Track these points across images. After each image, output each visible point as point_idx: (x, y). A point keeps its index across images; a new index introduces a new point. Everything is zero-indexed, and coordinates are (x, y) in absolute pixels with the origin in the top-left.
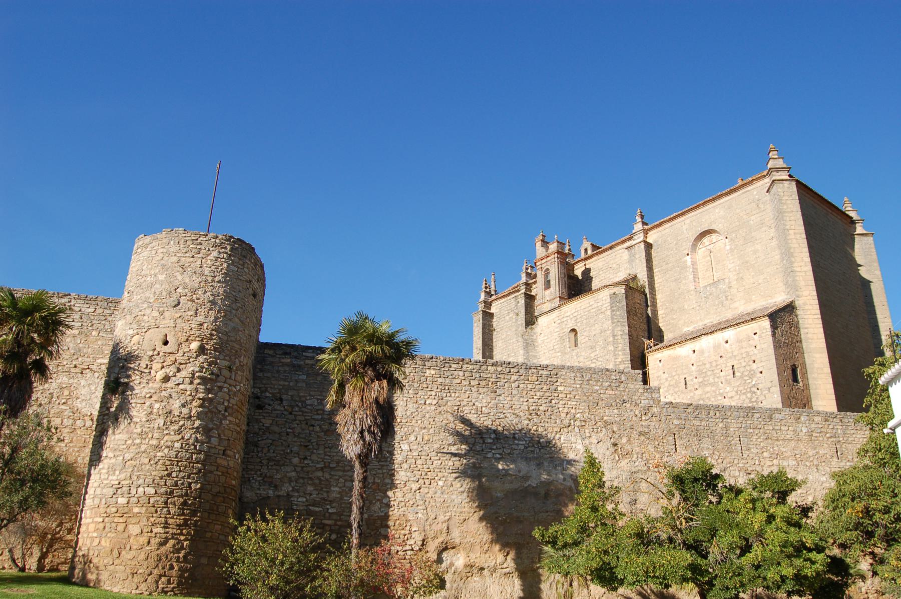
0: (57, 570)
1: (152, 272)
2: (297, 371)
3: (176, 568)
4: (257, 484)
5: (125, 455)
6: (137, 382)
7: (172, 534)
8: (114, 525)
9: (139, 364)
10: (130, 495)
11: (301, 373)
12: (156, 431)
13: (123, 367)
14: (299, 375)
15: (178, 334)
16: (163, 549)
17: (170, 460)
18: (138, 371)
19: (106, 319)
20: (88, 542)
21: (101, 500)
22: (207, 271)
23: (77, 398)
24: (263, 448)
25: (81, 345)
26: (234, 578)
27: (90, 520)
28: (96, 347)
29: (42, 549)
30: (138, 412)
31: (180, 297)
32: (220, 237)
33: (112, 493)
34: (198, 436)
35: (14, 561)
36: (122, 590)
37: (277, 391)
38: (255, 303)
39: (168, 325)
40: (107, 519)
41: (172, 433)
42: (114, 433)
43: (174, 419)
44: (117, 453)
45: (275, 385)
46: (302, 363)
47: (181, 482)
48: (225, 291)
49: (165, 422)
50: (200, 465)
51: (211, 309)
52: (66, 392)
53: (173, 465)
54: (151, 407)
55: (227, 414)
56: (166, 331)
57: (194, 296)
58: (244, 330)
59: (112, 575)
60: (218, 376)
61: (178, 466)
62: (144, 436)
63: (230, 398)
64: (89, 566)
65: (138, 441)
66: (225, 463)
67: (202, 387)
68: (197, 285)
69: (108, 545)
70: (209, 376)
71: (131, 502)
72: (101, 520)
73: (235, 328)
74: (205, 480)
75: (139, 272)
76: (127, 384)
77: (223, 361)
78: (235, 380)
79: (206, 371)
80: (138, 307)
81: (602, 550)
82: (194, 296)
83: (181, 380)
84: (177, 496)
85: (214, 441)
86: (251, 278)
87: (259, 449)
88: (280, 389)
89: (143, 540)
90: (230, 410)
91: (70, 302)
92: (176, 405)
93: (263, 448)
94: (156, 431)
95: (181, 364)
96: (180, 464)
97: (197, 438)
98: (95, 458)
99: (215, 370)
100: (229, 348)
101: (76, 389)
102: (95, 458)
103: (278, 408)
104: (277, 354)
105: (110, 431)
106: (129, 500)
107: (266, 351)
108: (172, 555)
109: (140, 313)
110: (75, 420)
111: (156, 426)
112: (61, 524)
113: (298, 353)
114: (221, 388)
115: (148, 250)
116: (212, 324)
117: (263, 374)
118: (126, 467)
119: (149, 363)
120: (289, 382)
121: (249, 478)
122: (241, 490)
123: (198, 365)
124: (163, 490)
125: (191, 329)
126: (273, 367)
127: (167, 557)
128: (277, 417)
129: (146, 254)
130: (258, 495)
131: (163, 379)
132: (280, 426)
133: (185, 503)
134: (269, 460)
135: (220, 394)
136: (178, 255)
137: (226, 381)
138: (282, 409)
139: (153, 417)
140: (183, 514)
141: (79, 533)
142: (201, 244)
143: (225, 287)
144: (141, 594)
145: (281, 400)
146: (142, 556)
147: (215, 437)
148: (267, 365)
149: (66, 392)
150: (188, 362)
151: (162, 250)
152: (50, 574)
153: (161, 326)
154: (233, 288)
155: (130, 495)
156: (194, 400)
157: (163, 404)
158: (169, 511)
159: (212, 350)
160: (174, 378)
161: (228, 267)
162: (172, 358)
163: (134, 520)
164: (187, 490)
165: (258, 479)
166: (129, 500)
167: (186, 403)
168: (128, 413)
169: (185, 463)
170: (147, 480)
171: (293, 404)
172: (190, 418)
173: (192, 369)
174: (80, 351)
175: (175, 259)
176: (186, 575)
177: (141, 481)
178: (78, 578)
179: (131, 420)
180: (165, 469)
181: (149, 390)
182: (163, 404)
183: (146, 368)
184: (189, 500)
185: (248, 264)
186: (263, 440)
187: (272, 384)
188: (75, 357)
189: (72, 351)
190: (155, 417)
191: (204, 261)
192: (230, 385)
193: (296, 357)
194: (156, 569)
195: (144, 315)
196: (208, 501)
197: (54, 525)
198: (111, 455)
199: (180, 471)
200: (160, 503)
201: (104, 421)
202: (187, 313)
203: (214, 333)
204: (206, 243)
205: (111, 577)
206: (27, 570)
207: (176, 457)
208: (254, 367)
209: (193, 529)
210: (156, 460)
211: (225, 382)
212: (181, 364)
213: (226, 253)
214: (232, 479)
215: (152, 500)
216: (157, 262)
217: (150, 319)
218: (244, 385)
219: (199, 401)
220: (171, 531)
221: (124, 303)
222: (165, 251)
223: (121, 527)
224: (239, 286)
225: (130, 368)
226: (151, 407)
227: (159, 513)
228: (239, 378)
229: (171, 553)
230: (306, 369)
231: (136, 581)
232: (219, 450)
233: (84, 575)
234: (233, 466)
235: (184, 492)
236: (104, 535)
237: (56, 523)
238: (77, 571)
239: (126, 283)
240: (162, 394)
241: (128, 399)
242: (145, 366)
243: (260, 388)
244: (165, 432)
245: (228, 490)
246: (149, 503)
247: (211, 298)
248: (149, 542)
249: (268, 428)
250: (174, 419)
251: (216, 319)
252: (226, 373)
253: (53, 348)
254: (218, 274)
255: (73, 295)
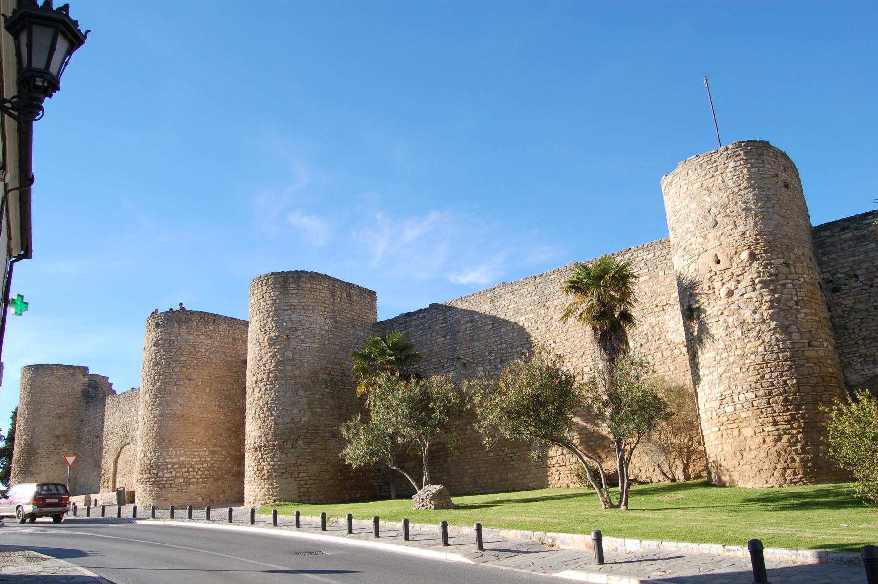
0: (701, 477)
1: (684, 205)
2: (863, 242)
3: (798, 460)
4: (859, 365)
5: (719, 370)
6: (706, 304)
7: (783, 430)
8: (729, 431)
9: (703, 288)
10: (734, 403)
11: (868, 243)
12: (737, 342)
13: (691, 295)
14: (867, 245)
15: (726, 250)
16: (779, 445)
17: (759, 364)
18: (704, 294)
19: (666, 259)
20: (714, 449)
21: (712, 412)
22: (730, 183)
23: (668, 332)
24: (853, 329)
25: (654, 287)
26: (843, 462)
27: (709, 431)
28: (666, 284)
29: (683, 461)
30: (716, 330)
31: (716, 216)
32: (730, 148)
33: (718, 405)
34: (778, 336)
35: (664, 474)
36: (754, 486)
37: (849, 268)
38: (791, 193)
39: (714, 246)
40: (722, 428)
41: (753, 340)
42: (703, 353)
43: (750, 327)
44: (711, 370)
45: (844, 263)
46: (865, 232)
47: (776, 381)
48: (754, 195)
49: (742, 332)
50: (789, 362)
51: (747, 216)
52: (657, 330)
53: (763, 368)
54: (725, 322)
55: (799, 307)
56: (714, 251)
57: (728, 211)
58: (788, 223)
59: (742, 475)
60: (777, 275)
61: (768, 368)
62: (729, 349)
63: (797, 292)
64: (720, 469)
65: (725, 355)
66: (814, 354)
67: (765, 290)
68: (726, 200)
69: (730, 449)
70: (769, 278)
71: (737, 409)
72: (717, 429)
73: (778, 225)
74: (799, 375)
75: (673, 209)
76: (699, 308)
77: (777, 260)
78: (796, 273)
79: (764, 275)
80: (684, 239)
81: (258, 446)
82: (728, 211)
83: (743, 290)
84: (777, 395)
85: (796, 336)
86: (775, 171)
87: (850, 331)
88: (851, 266)
89: (759, 439)
90: (801, 303)
91: (632, 255)
92: (747, 314)
93: (853, 329)
94: (737, 342)
95: (738, 276)
96: (769, 365)
97: (777, 338)
98: (695, 378)
99: (772, 271)
100: (778, 246)
101: (664, 324)
102: (695, 378)
103: (856, 285)
104: (835, 233)
105: (700, 353)
106: (735, 408)
107: (822, 234)
108: (789, 448)
109: (687, 244)
110: (672, 351)
111: (736, 337)
112: (691, 439)
113: (858, 224)
114: (784, 285)
115: (673, 186)
116: (753, 230)
117: (828, 257)
118: (723, 379)
119: (710, 285)
120: (858, 256)
121: (849, 362)
122: (844, 375)
123: (754, 272)
124: (762, 392)
125: (736, 241)
126: (836, 246)
127: (786, 452)
128: (858, 294)
129: (673, 191)
130: (865, 376)
131: (727, 294)
132: (864, 303)
133: (786, 400)
134: (864, 339)
135: (785, 291)
136: (699, 180)
137: (786, 277)
138: (861, 285)
139: (731, 330)
140: (788, 410)
141: (704, 443)
142: (716, 162)
143: (753, 191)
144: (772, 487)
145: (856, 276)
146: (763, 454)
147: (795, 332)
148: (828, 247)
149: (657, 330)
150: (744, 272)
151: (684, 182)
152: (695, 481)
153: (709, 248)
154: (761, 189)
155: (734, 403)
156: (762, 304)
157: (735, 316)
158: (773, 410)
159: (762, 253)
160: (736, 291)
161: (748, 171)
162: (728, 273)
163: (745, 424)
164: (785, 387)
165: (859, 360)
166: (735, 408)
167: (756, 309)
168: (708, 333)
169: (774, 363)
170: (744, 387)
171: (871, 276)
172: (764, 321)
173: (750, 277)
174: (655, 292)
175: (698, 185)
176: (810, 465)
177: (739, 389)
178: (716, 481)
179: (713, 338)
180: (757, 373)
181: (719, 308)
182: (735, 316)
183: (710, 289)
184: (790, 396)
185: (768, 160)
186: (850, 321)
187: (841, 264)
188: (654, 298)
189: (650, 295)
190: (732, 330)
191: (724, 176)
192: (793, 280)
193: (856, 229)
194: (779, 463)
195: (691, 244)
196: (808, 394)
197: (686, 441)
198: (707, 372)
199: (772, 372)
200: (763, 404)
201: (692, 345)
202: (727, 229)
203: (758, 237)
204: (720, 159)
205: (741, 476)
206: (677, 481)
207: (764, 360)
208: (816, 254)
209: (802, 422)
210: (747, 368)
211: (786, 279)
212: (738, 276)
213: (742, 159)
214: (827, 368)
215: (755, 403)
216: (685, 195)
217: (697, 246)
218: (808, 275)
219: (767, 304)
220: (781, 427)
221: (673, 240)
222: (687, 181)
223: (736, 432)
224: (766, 184)
225: (697, 293)
226: (725, 322)
227: (765, 413)
228: (800, 270)
229: (788, 447)
230: (872, 237)
231: (764, 476)
232: (804, 343)
233: (719, 478)
234: (823, 354)
235: (782, 390)
236: (724, 441)
237: (687, 438)
238: (713, 475)
239: (668, 222)
240: (731, 308)
241: (704, 321)
242: (708, 288)
243: (829, 272)
244: (746, 341)
245: (826, 379)
246: (753, 406)
247: (744, 207)
248: (764, 441)
249: (851, 308)
250: (750, 327)
251: (756, 223)
252: (784, 270)
253: (584, 304)
254: (742, 182)
255: (632, 248)
